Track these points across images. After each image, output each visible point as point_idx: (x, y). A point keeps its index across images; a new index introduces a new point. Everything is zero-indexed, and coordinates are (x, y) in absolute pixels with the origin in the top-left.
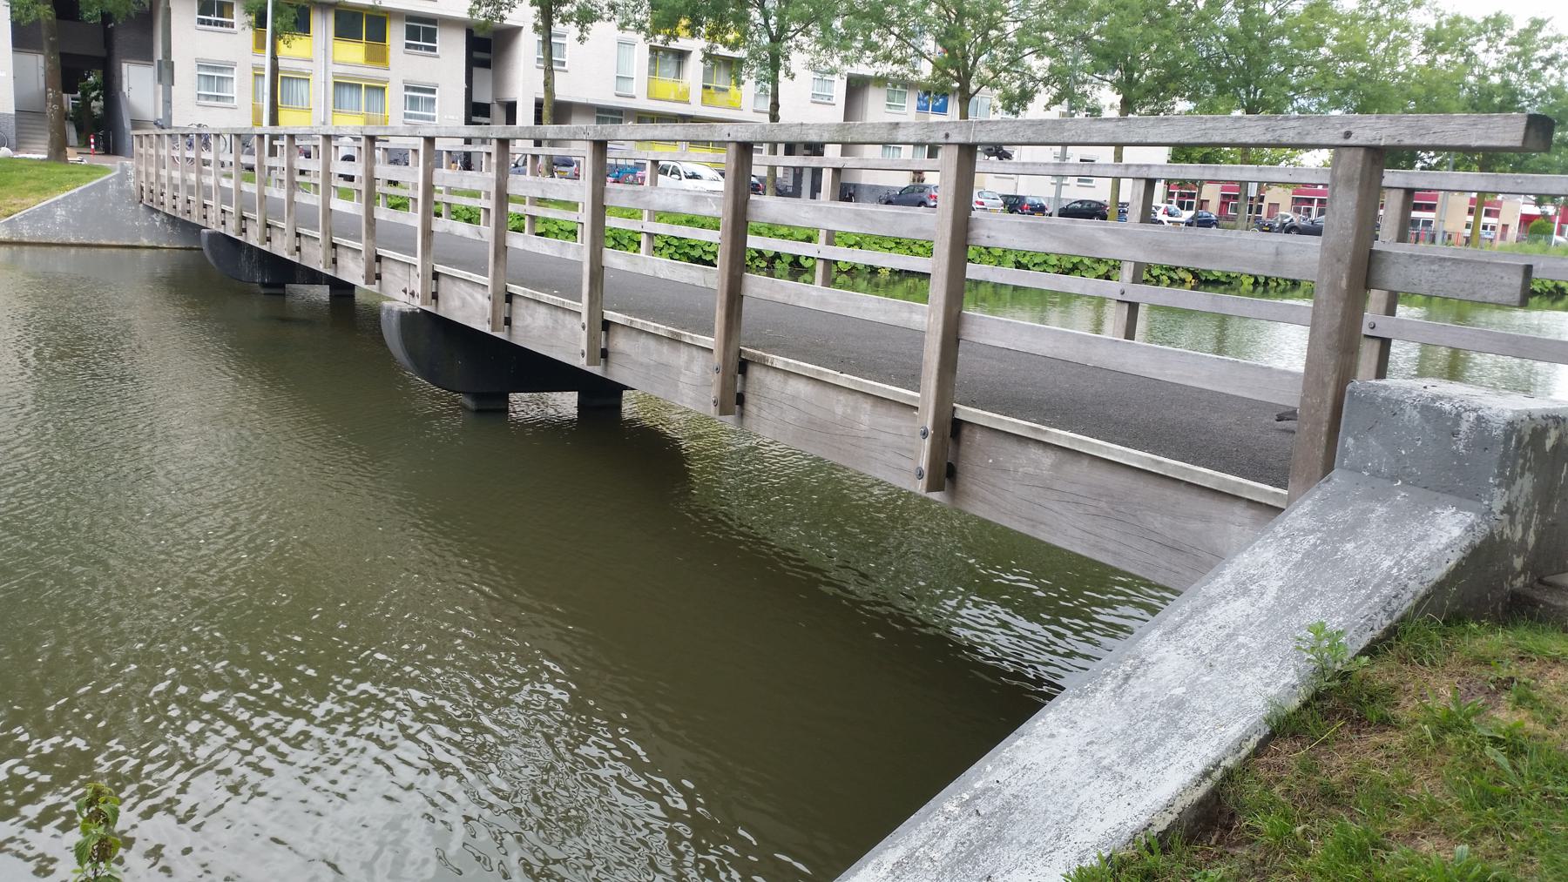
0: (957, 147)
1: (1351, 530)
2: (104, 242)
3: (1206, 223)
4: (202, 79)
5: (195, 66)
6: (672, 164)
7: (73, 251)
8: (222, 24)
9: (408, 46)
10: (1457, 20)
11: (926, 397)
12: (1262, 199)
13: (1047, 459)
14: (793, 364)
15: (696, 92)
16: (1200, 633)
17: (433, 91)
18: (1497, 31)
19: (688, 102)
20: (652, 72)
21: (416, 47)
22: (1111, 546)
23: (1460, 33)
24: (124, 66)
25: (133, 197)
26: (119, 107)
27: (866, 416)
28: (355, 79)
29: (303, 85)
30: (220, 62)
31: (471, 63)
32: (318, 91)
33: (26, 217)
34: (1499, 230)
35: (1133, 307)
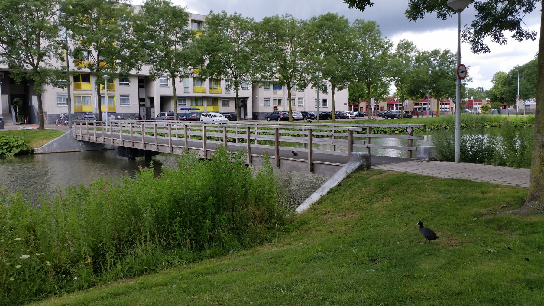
1: (351, 165)
2: (66, 151)
3: (361, 115)
5: (56, 95)
6: (208, 113)
7: (59, 154)
9: (120, 84)
10: (424, 53)
11: (309, 161)
12: (378, 106)
13: (324, 166)
14: (288, 158)
15: (208, 90)
16: (338, 174)
17: (129, 96)
18: (436, 55)
19: (206, 93)
20: (194, 84)
21: (123, 84)
23: (426, 56)
24: (33, 97)
25: (74, 138)
26: (33, 111)
27: (300, 164)
29: (89, 98)
31: (140, 86)
33: (46, 146)
34: (450, 108)
35: (335, 146)
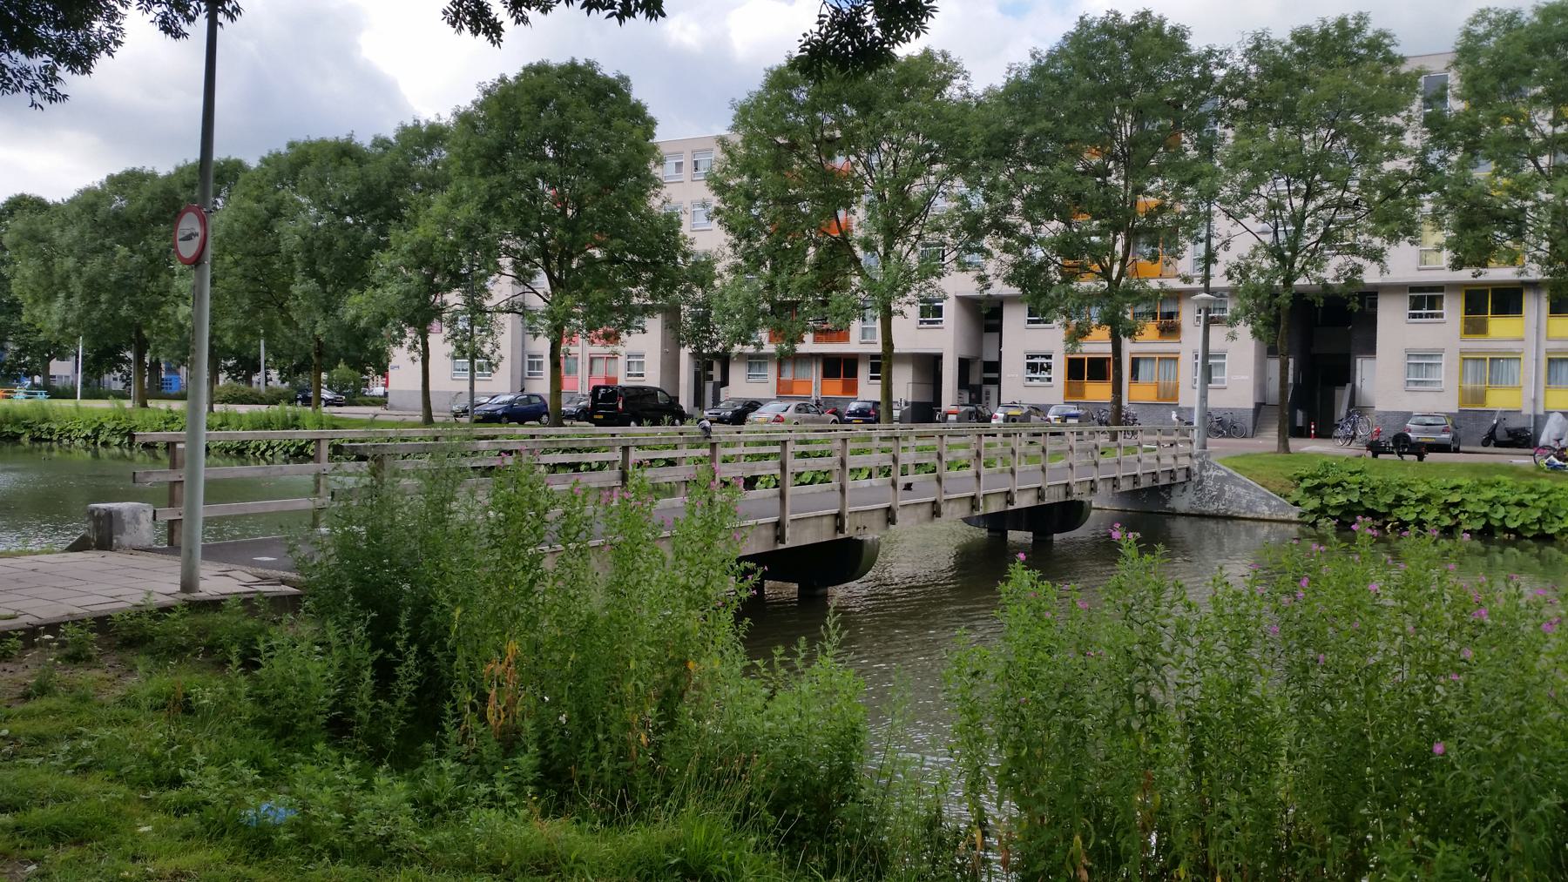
0: (820, 360)
4: (1412, 367)
8: (1432, 316)
22: (483, 444)
24: (1359, 360)
28: (1504, 353)
29: (1514, 365)
30: (1426, 350)
32: (1529, 370)
